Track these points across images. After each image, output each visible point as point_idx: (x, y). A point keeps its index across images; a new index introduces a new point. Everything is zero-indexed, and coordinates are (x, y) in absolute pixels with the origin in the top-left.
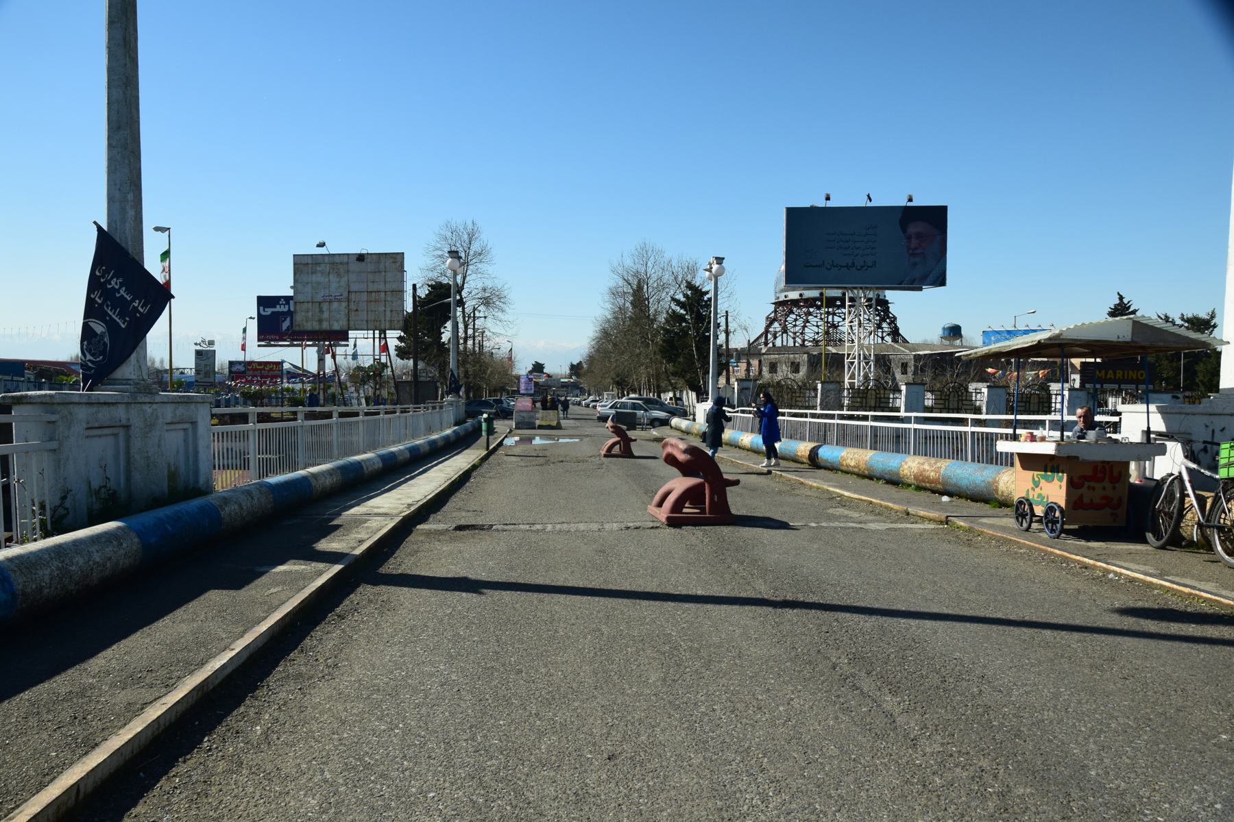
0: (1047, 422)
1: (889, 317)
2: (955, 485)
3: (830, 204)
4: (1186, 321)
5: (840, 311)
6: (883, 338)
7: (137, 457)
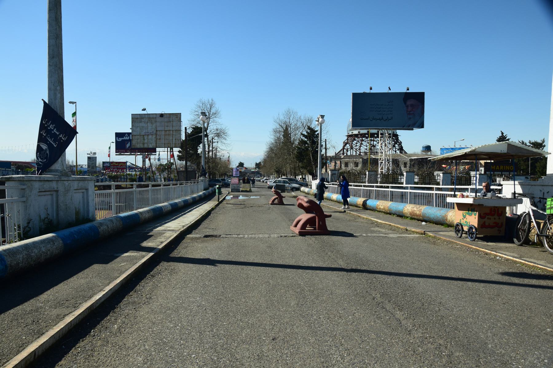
0: (469, 189)
1: (398, 142)
3: (372, 91)
5: (376, 139)
6: (396, 151)
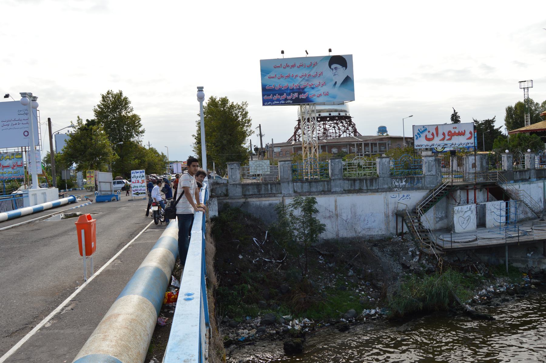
0: (355, 145)
5: (329, 123)
6: (350, 134)
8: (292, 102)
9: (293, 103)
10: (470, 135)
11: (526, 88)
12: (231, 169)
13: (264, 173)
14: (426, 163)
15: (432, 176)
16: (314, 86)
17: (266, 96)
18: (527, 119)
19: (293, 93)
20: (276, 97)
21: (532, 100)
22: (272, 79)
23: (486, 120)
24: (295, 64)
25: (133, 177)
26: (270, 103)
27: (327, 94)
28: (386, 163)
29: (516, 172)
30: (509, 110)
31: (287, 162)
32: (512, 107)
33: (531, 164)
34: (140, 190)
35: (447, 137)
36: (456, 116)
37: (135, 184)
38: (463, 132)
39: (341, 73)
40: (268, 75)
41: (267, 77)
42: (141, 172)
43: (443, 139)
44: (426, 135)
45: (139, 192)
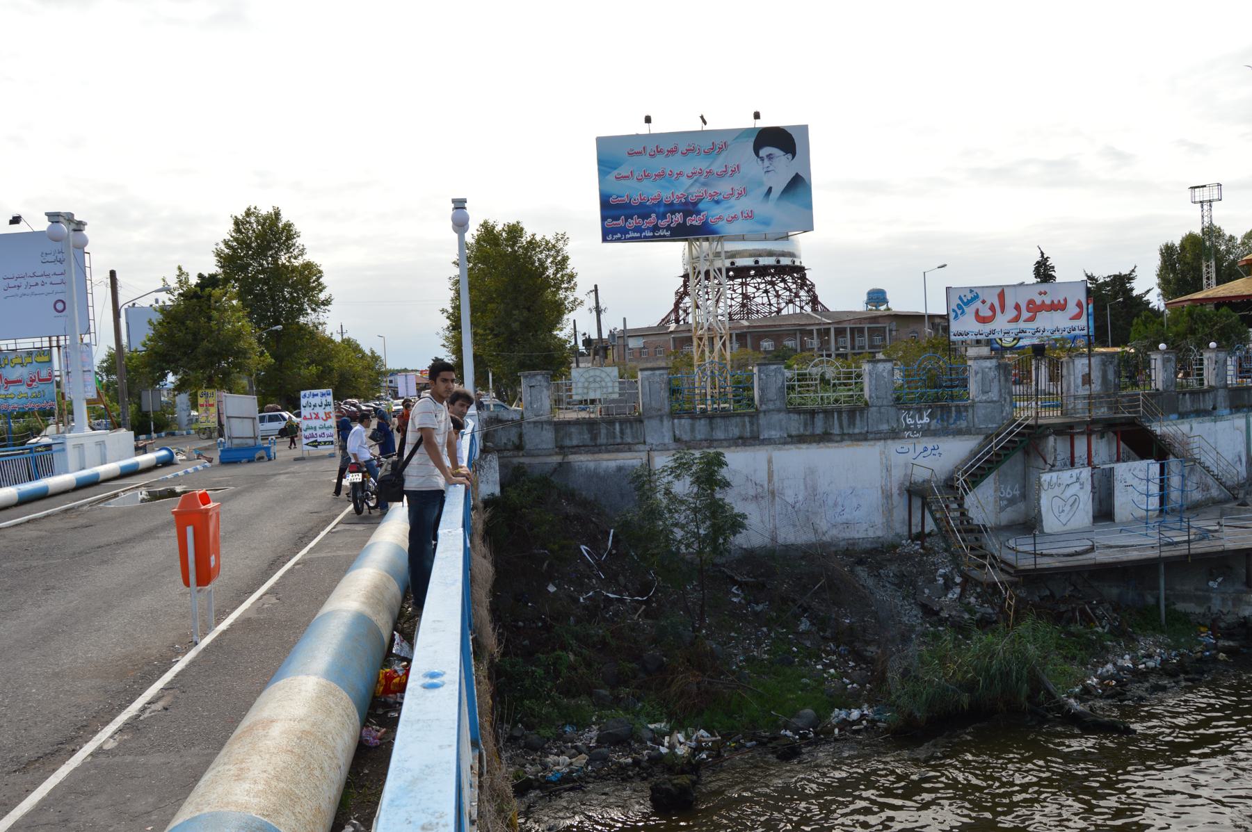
0: (815, 332)
2: (458, 447)
4: (1229, 635)
5: (755, 281)
6: (802, 308)
7: (272, 480)
8: (669, 233)
9: (672, 235)
10: (1077, 310)
11: (1207, 201)
12: (531, 387)
13: (605, 396)
14: (977, 373)
15: (991, 404)
16: (721, 197)
17: (610, 220)
18: (1208, 273)
19: (673, 213)
20: (632, 223)
21: (1219, 228)
22: (623, 182)
23: (1115, 276)
24: (676, 147)
25: (304, 407)
26: (619, 235)
27: (749, 216)
28: (885, 374)
29: (1184, 394)
30: (1168, 252)
31: (658, 372)
32: (1174, 245)
33: (1217, 375)
34: (320, 436)
35: (1026, 314)
36: (1046, 266)
37: (310, 421)
38: (1062, 302)
39: (782, 168)
40: (615, 173)
41: (611, 177)
42: (323, 395)
43: (1016, 319)
44: (978, 310)
45: (319, 439)
